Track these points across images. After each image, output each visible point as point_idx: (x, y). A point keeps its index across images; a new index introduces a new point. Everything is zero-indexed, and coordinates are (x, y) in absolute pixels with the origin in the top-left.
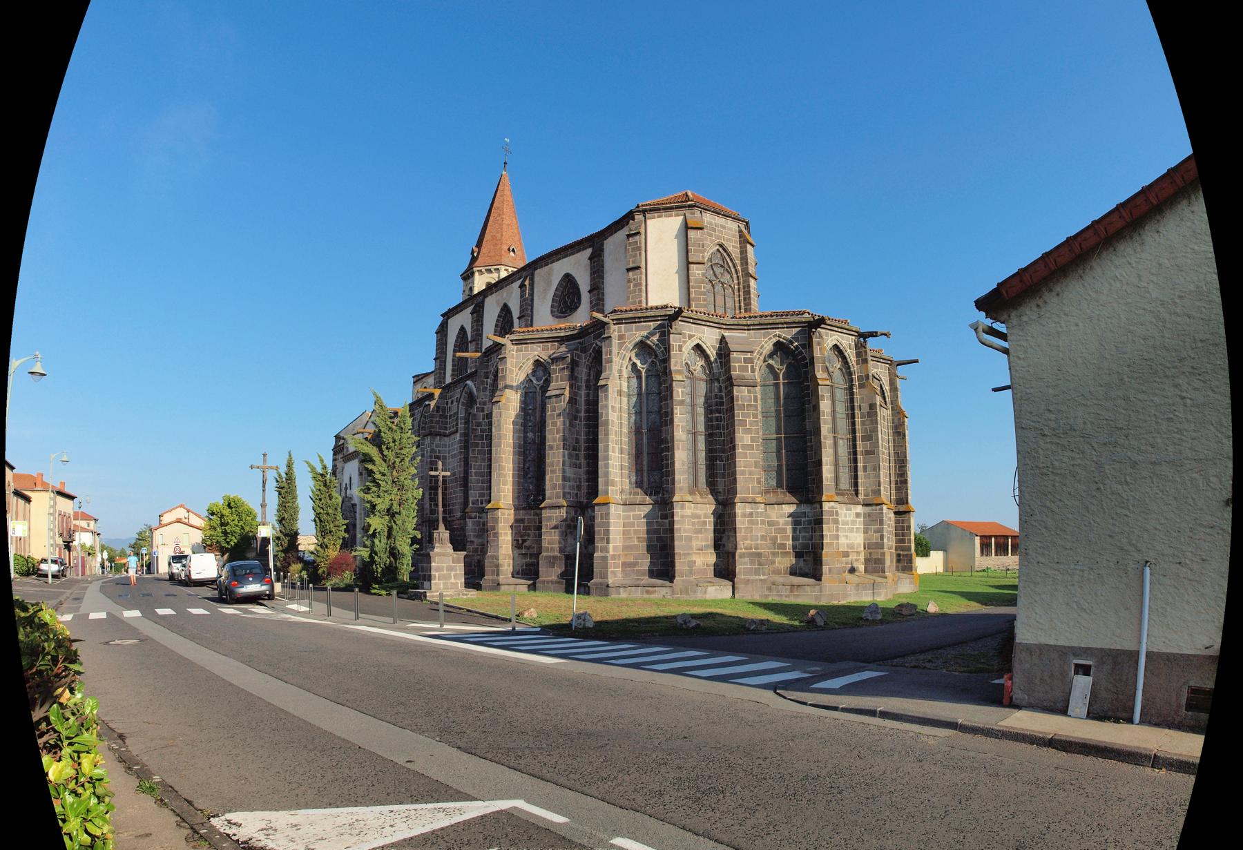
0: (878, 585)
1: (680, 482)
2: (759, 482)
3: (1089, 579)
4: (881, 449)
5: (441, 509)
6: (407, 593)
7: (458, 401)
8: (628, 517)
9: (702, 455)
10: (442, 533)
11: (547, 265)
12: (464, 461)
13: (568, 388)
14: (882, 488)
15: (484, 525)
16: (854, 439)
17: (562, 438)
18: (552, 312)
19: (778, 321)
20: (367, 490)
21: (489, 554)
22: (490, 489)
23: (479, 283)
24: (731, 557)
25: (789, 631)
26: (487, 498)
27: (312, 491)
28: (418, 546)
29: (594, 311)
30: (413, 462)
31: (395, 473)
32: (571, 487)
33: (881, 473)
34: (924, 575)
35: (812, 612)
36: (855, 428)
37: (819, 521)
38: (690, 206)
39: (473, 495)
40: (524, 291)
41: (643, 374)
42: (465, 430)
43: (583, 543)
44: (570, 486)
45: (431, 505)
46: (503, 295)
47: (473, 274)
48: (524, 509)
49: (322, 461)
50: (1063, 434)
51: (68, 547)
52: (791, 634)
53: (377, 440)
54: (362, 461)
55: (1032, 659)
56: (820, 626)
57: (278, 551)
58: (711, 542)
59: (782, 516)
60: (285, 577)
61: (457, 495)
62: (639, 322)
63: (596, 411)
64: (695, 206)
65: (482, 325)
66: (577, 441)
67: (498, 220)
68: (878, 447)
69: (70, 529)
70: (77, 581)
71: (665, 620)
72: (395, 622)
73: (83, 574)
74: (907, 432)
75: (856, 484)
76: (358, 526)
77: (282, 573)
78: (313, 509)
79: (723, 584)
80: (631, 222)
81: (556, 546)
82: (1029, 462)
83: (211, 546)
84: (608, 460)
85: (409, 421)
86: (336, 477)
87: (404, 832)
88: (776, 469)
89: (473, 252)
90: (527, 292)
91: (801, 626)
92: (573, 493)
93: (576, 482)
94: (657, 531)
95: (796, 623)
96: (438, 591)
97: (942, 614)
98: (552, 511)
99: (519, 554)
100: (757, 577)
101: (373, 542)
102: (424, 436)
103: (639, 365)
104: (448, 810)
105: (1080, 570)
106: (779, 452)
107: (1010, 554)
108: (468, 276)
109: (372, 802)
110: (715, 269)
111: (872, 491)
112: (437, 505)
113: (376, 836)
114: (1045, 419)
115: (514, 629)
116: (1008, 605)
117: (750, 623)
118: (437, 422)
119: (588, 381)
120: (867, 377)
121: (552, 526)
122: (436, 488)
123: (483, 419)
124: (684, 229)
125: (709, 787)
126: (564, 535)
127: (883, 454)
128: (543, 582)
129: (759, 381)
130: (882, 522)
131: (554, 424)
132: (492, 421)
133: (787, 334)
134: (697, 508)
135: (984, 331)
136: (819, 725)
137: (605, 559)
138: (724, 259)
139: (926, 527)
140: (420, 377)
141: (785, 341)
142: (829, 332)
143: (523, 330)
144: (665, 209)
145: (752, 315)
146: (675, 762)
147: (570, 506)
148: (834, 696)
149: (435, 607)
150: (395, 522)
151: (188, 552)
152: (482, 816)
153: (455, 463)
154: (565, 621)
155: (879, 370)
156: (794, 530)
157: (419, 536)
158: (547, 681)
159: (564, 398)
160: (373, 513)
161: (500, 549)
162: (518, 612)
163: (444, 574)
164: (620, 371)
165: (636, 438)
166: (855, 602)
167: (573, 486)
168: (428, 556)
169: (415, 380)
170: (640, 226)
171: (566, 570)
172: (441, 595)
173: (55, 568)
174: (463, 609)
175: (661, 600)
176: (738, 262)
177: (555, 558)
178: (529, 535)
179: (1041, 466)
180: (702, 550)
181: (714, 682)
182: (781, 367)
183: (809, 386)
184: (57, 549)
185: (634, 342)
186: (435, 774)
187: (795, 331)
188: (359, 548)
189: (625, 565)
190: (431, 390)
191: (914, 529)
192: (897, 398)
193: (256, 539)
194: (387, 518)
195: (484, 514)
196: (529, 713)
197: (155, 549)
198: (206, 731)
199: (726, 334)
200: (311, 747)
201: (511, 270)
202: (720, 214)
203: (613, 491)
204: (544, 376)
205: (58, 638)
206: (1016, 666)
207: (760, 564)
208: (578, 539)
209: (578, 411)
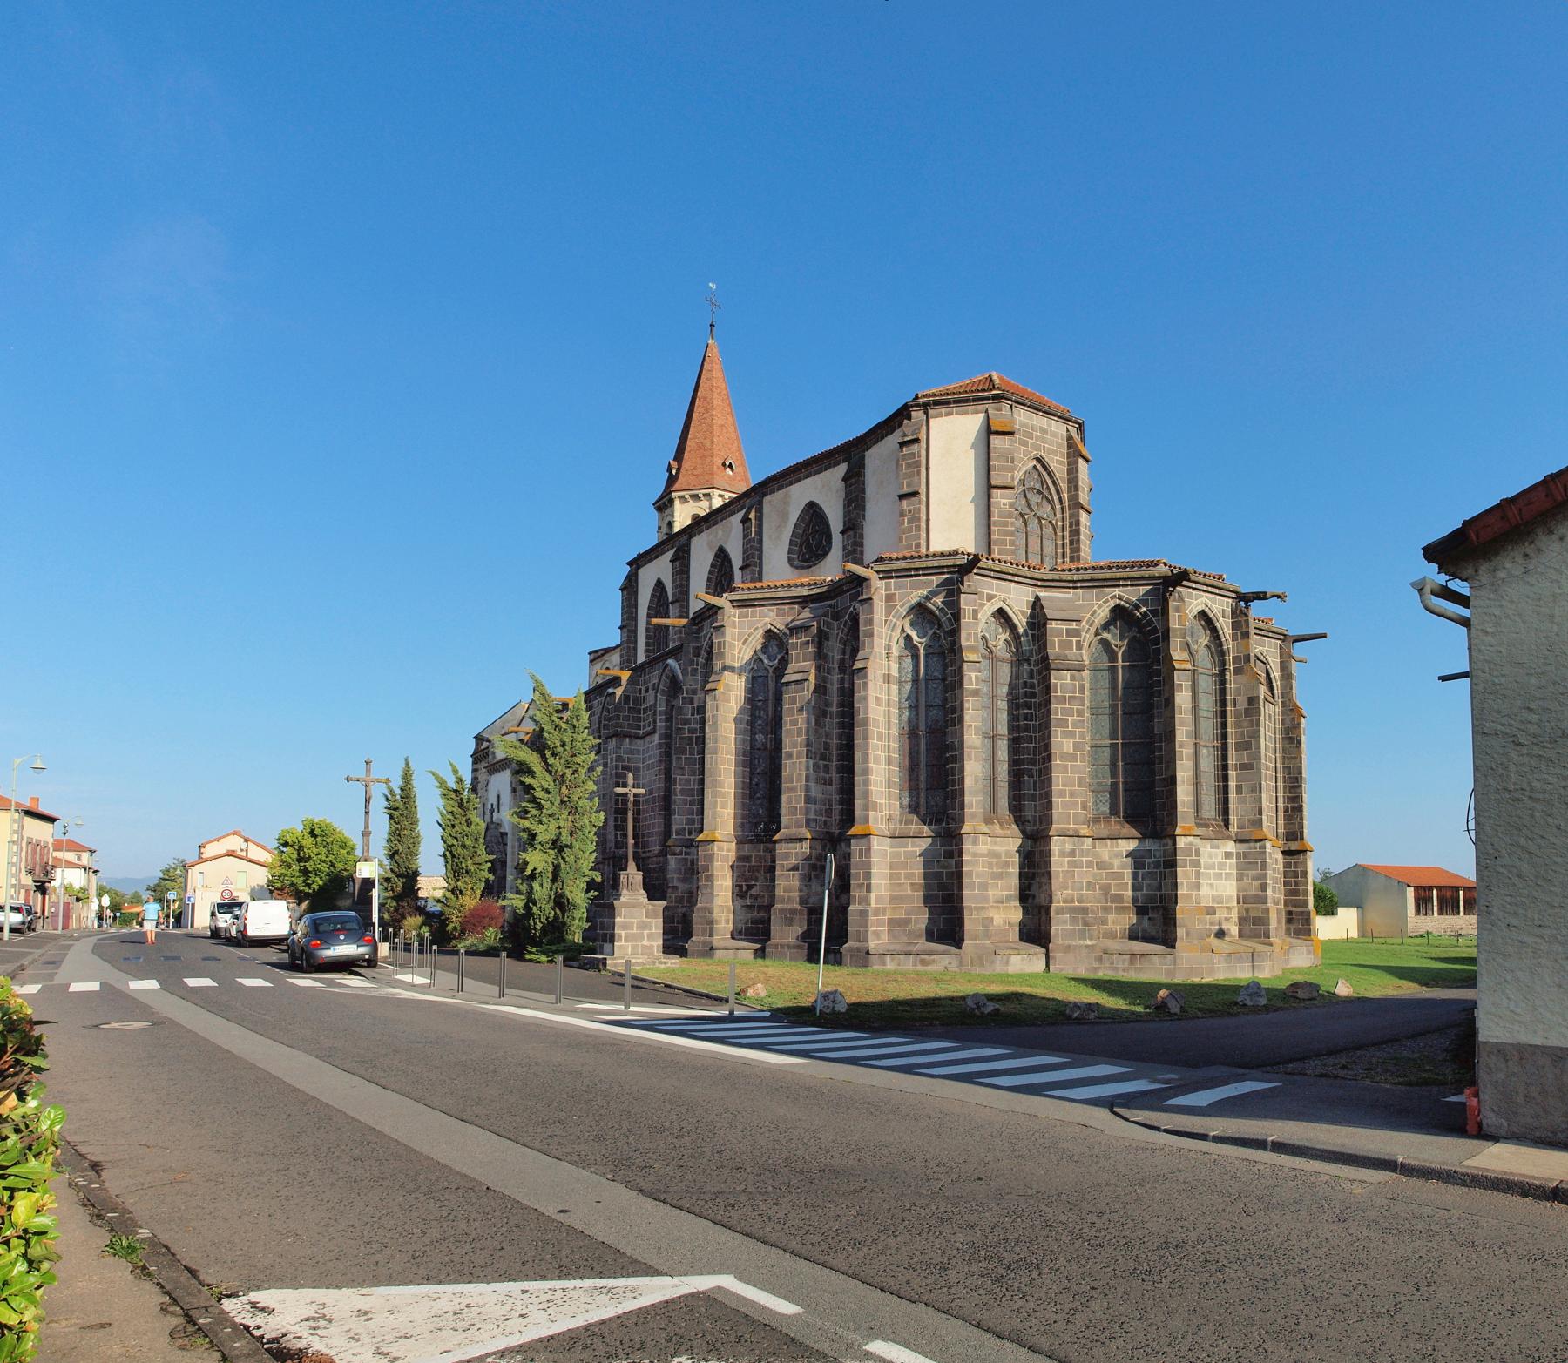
0: (1259, 956)
1: (971, 807)
2: (1084, 808)
4: (1263, 761)
5: (631, 841)
6: (577, 960)
7: (656, 688)
8: (898, 855)
9: (1003, 769)
10: (632, 875)
11: (781, 488)
13: (813, 671)
14: (1264, 817)
15: (692, 864)
16: (1224, 747)
17: (804, 743)
18: (790, 560)
19: (1118, 575)
20: (523, 813)
21: (699, 905)
22: (702, 813)
23: (682, 516)
26: (697, 826)
27: (441, 814)
28: (597, 893)
31: (564, 789)
33: (1264, 796)
35: (1163, 993)
37: (1171, 864)
38: (995, 398)
39: (678, 822)
40: (748, 528)
43: (833, 891)
44: (816, 811)
45: (616, 834)
47: (671, 501)
48: (751, 841)
49: (456, 771)
50: (1550, 742)
51: (42, 888)
53: (537, 742)
54: (516, 773)
55: (1507, 1067)
56: (1175, 1014)
58: (1015, 892)
59: (1117, 855)
60: (395, 935)
61: (655, 823)
63: (852, 705)
65: (688, 579)
66: (827, 746)
67: (705, 418)
68: (1260, 759)
69: (47, 863)
70: (54, 937)
71: (950, 1002)
73: (65, 926)
74: (1303, 738)
75: (1226, 812)
76: (509, 863)
77: (391, 930)
78: (442, 839)
80: (906, 422)
81: (796, 894)
82: (1492, 782)
83: (282, 889)
85: (585, 716)
86: (477, 794)
87: (541, 1327)
88: (1108, 788)
89: (670, 469)
91: (1146, 1013)
92: (820, 820)
93: (825, 805)
94: (938, 875)
95: (1140, 1009)
96: (623, 958)
97: (1359, 998)
98: (791, 845)
100: (1081, 942)
101: (531, 887)
102: (607, 738)
104: (615, 1291)
106: (1113, 764)
107: (1462, 913)
108: (664, 504)
109: (497, 1275)
110: (1029, 495)
111: (1249, 820)
112: (625, 835)
113: (495, 1332)
114: (1521, 721)
115: (732, 1013)
116: (1462, 987)
118: (626, 718)
119: (842, 661)
120: (1247, 658)
121: (790, 866)
122: (625, 812)
123: (693, 715)
124: (984, 435)
125: (1017, 1258)
126: (807, 879)
127: (1267, 768)
128: (776, 946)
129: (1087, 662)
130: (1263, 866)
131: (794, 723)
132: (704, 718)
133: (1131, 595)
134: (995, 843)
135: (1433, 593)
136: (1180, 1163)
137: (864, 914)
138: (1043, 480)
139: (1330, 873)
140: (600, 653)
142: (1195, 592)
144: (958, 402)
145: (1080, 566)
146: (965, 1217)
147: (816, 839)
148: (1202, 1118)
149: (619, 980)
150: (563, 859)
151: (243, 897)
152: (667, 1302)
153: (653, 776)
154: (806, 1002)
156: (1135, 876)
157: (599, 879)
159: (808, 686)
160: (532, 846)
163: (634, 934)
164: (888, 647)
165: (910, 744)
166: (1225, 980)
168: (612, 907)
170: (919, 429)
171: (809, 930)
172: (628, 963)
173: (16, 918)
174: (659, 983)
176: (1064, 486)
177: (793, 911)
178: (756, 879)
179: (1512, 787)
180: (1002, 902)
181: (1021, 1095)
182: (1119, 643)
183: (1160, 670)
184: (23, 892)
185: (908, 605)
186: (599, 1232)
187: (1143, 590)
188: (509, 895)
190: (615, 672)
191: (1313, 876)
192: (1291, 688)
193: (353, 880)
194: (552, 852)
195: (693, 849)
197: (190, 893)
198: (244, 1160)
199: (1043, 593)
200: (411, 1186)
201: (727, 495)
202: (1040, 411)
203: (876, 819)
204: (780, 652)
205: (10, 1018)
206: (1483, 1076)
207: (1086, 923)
208: (827, 885)
209: (828, 704)
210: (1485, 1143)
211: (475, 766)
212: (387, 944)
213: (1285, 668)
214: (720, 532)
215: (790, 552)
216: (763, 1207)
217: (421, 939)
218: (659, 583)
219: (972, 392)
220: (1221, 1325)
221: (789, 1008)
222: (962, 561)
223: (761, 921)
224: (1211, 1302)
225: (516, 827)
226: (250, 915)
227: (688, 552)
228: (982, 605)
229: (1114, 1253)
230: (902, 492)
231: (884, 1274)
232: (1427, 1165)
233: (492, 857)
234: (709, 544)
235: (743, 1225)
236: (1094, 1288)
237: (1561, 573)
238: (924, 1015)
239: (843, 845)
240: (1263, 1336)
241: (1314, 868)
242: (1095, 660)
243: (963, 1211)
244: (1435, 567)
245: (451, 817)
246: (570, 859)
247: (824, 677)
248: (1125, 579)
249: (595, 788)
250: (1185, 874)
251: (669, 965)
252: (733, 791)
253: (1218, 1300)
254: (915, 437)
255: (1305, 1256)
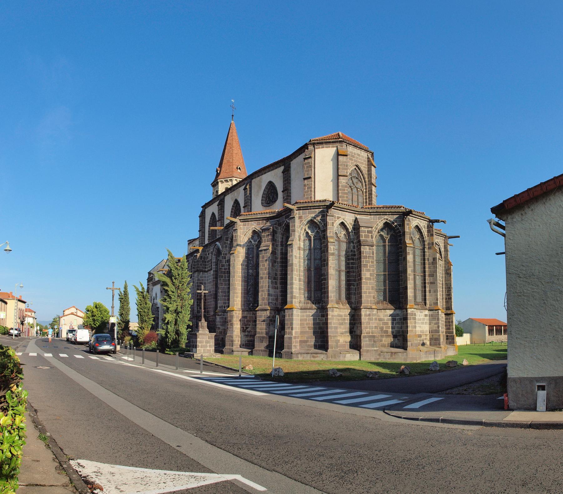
0: (437, 352)
2: (374, 298)
3: (541, 345)
4: (438, 281)
5: (203, 311)
6: (183, 354)
7: (212, 253)
8: (303, 316)
9: (343, 283)
10: (203, 323)
11: (259, 176)
12: (215, 285)
13: (271, 246)
14: (439, 302)
15: (225, 319)
16: (425, 276)
17: (268, 273)
18: (262, 203)
19: (386, 211)
21: (228, 335)
22: (229, 300)
23: (222, 188)
24: (358, 337)
25: (390, 378)
26: (227, 305)
27: (137, 300)
28: (190, 330)
29: (285, 203)
30: (188, 286)
31: (179, 291)
32: (273, 300)
33: (438, 294)
34: (461, 346)
35: (403, 367)
36: (425, 270)
37: (405, 319)
38: (340, 142)
40: (246, 192)
41: (312, 238)
42: (216, 268)
44: (272, 299)
46: (235, 194)
47: (218, 183)
48: (247, 311)
49: (142, 285)
50: (529, 277)
51: (22, 323)
52: (391, 379)
53: (169, 274)
54: (162, 285)
55: (516, 385)
56: (407, 374)
57: (119, 330)
59: (386, 316)
60: (122, 343)
61: (211, 303)
62: (310, 209)
64: (343, 142)
65: (224, 211)
66: (276, 274)
70: (25, 339)
72: (177, 369)
73: (28, 335)
74: (452, 273)
75: (425, 299)
76: (160, 318)
77: (121, 341)
79: (355, 352)
80: (306, 150)
81: (264, 331)
82: (512, 290)
83: (87, 326)
84: (292, 285)
85: (186, 264)
86: (149, 293)
88: (383, 291)
89: (217, 171)
90: (248, 192)
93: (275, 297)
94: (319, 324)
95: (394, 373)
98: (262, 312)
99: (244, 335)
100: (373, 349)
101: (167, 327)
102: (194, 272)
103: (310, 233)
104: (197, 477)
105: (537, 341)
106: (385, 282)
107: (503, 334)
108: (215, 184)
110: (353, 180)
112: (201, 308)
113: (155, 487)
114: (521, 270)
115: (240, 375)
116: (503, 359)
117: (369, 374)
118: (201, 265)
119: (282, 242)
120: (433, 243)
121: (262, 320)
122: (201, 299)
124: (336, 155)
126: (268, 325)
128: (257, 350)
129: (375, 243)
130: (438, 319)
131: (264, 265)
137: (290, 338)
138: (358, 174)
141: (390, 222)
142: (414, 218)
143: (246, 214)
144: (326, 143)
145: (373, 207)
146: (329, 454)
149: (198, 362)
150: (179, 317)
151: (76, 328)
152: (216, 483)
153: (211, 286)
154: (268, 372)
155: (439, 240)
156: (392, 323)
157: (191, 324)
158: (257, 405)
159: (269, 251)
160: (168, 312)
161: (234, 332)
162: (243, 367)
164: (300, 236)
167: (274, 299)
168: (196, 335)
169: (189, 242)
170: (311, 153)
172: (202, 356)
173: (16, 332)
174: (213, 364)
175: (321, 361)
176: (366, 176)
177: (263, 337)
178: (249, 325)
179: (518, 292)
180: (343, 334)
182: (387, 236)
184: (18, 324)
185: (307, 220)
186: (192, 455)
187: (395, 217)
188: (160, 330)
189: (301, 342)
190: (197, 247)
191: (455, 323)
193: (109, 323)
194: (175, 314)
195: (226, 314)
196: (247, 423)
197: (61, 326)
199: (358, 217)
200: (127, 431)
201: (238, 180)
202: (357, 147)
203: (295, 302)
204: (258, 239)
206: (509, 389)
207: (374, 342)
208: (276, 327)
209: (276, 258)
210: (510, 412)
211: (148, 283)
212: (119, 346)
213: (445, 248)
214: (236, 194)
215: (262, 200)
216: (252, 449)
217: (130, 344)
218: (213, 214)
219: (332, 139)
220: (423, 488)
221: (262, 374)
222: (328, 204)
223: (251, 341)
224: (420, 480)
225: (162, 305)
226: (78, 334)
227: (224, 202)
228: (335, 221)
229: (385, 465)
230: (305, 177)
231: (296, 474)
232: (492, 422)
233: (154, 316)
234: (232, 199)
235: (244, 456)
236: (377, 479)
237: (532, 221)
238: (313, 377)
239: (282, 312)
240: (438, 490)
241: (455, 320)
242: (378, 242)
243: (328, 452)
244: (494, 215)
245: (140, 302)
246: (181, 317)
247: (275, 248)
248: (389, 212)
249: (190, 291)
250: (411, 322)
251: (217, 357)
252: (241, 291)
253: (422, 479)
254: (310, 156)
255: (452, 459)
